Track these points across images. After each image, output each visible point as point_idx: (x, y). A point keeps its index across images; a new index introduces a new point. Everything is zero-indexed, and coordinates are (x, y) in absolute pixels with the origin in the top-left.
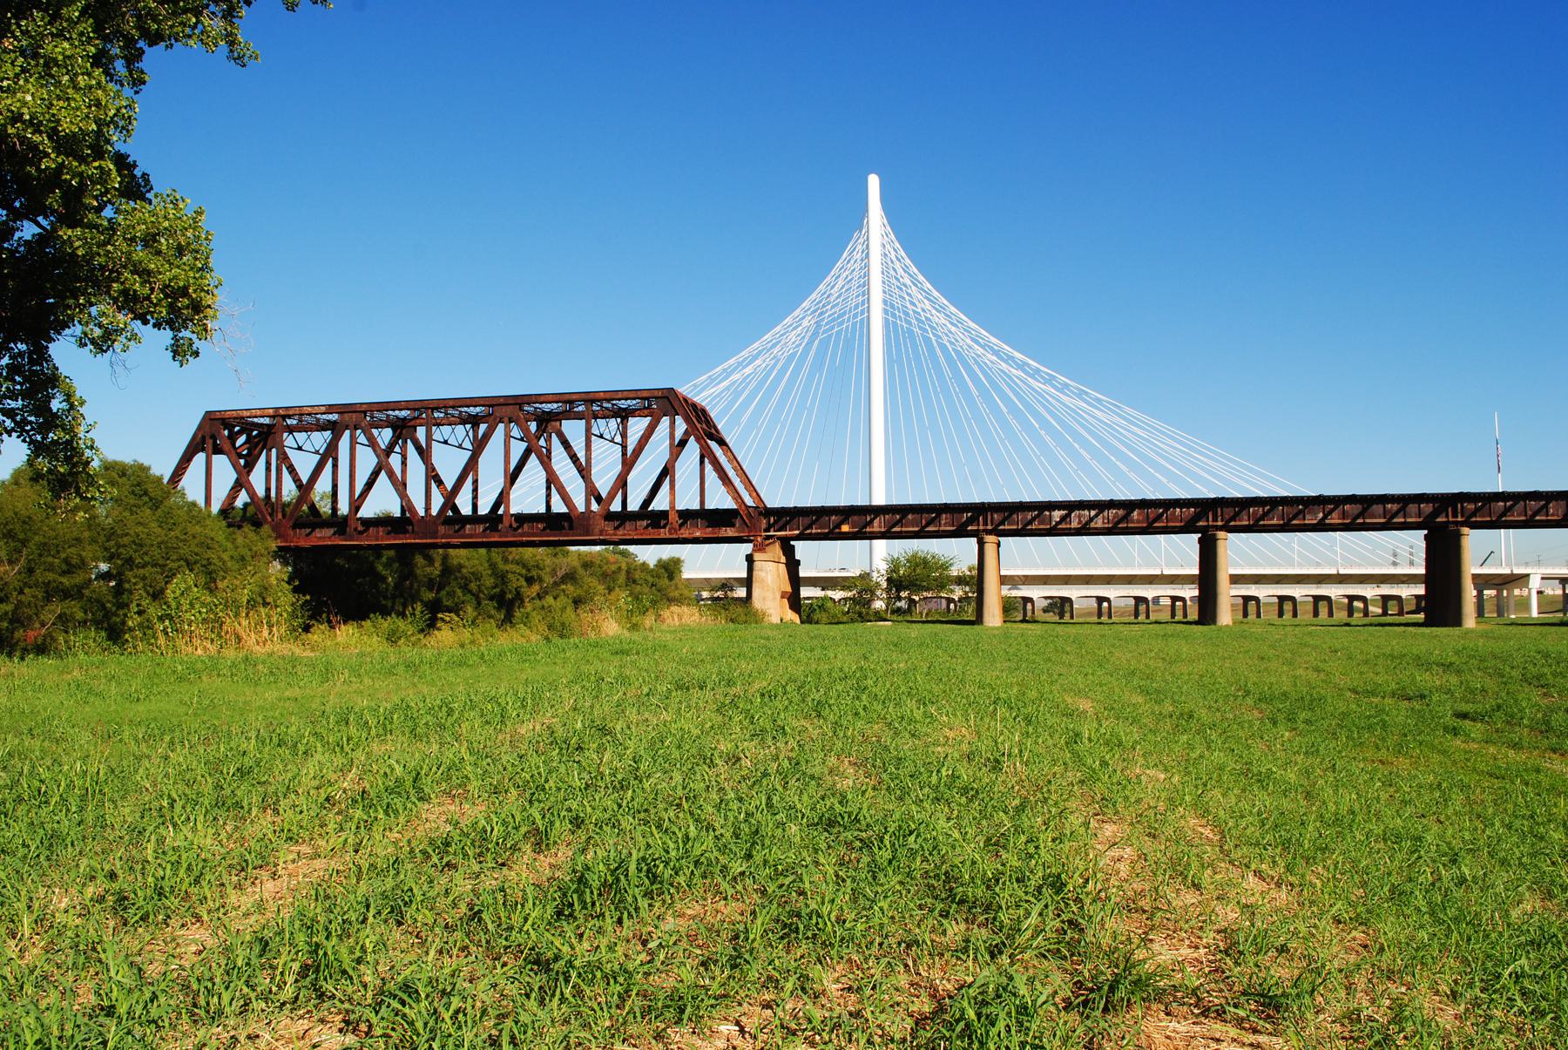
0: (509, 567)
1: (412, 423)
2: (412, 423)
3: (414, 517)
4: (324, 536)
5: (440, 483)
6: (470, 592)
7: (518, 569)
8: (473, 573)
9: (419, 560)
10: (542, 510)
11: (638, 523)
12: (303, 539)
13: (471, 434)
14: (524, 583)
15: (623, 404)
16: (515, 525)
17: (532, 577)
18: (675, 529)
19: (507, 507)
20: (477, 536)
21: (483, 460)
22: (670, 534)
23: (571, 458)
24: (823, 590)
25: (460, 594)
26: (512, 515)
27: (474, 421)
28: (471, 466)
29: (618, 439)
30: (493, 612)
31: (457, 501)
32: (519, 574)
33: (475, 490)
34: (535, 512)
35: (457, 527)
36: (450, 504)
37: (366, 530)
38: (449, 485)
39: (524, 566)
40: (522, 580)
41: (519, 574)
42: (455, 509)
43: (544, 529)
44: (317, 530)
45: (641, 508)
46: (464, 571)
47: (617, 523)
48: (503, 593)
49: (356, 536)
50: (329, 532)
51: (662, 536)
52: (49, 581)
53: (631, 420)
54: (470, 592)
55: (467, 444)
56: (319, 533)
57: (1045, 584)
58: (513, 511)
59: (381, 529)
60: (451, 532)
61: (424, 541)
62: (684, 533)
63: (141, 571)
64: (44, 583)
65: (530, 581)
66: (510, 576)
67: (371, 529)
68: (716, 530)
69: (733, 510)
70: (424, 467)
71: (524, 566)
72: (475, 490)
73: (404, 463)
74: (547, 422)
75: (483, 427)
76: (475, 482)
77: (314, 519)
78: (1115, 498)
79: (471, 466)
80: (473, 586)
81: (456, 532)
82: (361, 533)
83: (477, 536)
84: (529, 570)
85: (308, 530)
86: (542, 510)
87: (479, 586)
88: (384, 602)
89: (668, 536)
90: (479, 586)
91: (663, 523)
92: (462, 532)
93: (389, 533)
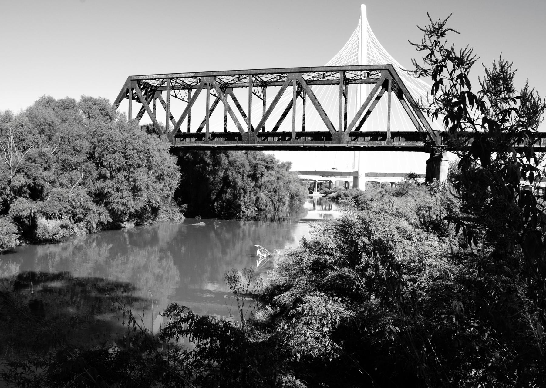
0: (258, 162)
1: (231, 86)
2: (231, 86)
3: (242, 132)
4: (190, 142)
5: (172, 118)
6: (240, 173)
7: (263, 163)
8: (241, 164)
9: (223, 156)
10: (223, 131)
11: (366, 138)
12: (180, 143)
13: (188, 94)
14: (266, 170)
15: (265, 78)
16: (211, 138)
17: (269, 167)
18: (390, 142)
19: (207, 129)
20: (274, 143)
21: (193, 109)
22: (388, 144)
23: (237, 106)
24: (323, 177)
25: (235, 174)
26: (210, 133)
27: (189, 88)
28: (187, 111)
29: (262, 97)
30: (250, 183)
31: (180, 128)
32: (263, 165)
33: (189, 121)
34: (317, 131)
35: (263, 138)
36: (177, 130)
37: (214, 138)
38: (177, 120)
39: (265, 161)
40: (264, 168)
41: (263, 165)
42: (179, 131)
43: (312, 140)
44: (187, 138)
45: (197, 131)
46: (237, 163)
47: (353, 138)
48: (255, 174)
49: (210, 142)
50: (193, 139)
51: (383, 145)
52: (65, 160)
53: (268, 88)
54: (240, 173)
55: (186, 99)
56: (188, 140)
57: (385, 176)
58: (211, 131)
59: (221, 139)
60: (260, 140)
61: (248, 145)
62: (396, 144)
63: (113, 156)
64: (62, 160)
65: (268, 168)
66: (259, 166)
67: (216, 138)
68: (415, 143)
69: (237, 133)
70: (165, 112)
71: (265, 161)
72: (189, 121)
73: (155, 108)
74: (225, 88)
75: (194, 91)
76: (189, 117)
77: (179, 134)
78: (381, 131)
79: (187, 111)
80: (241, 170)
81: (262, 140)
82: (211, 140)
83: (274, 143)
84: (267, 163)
85: (182, 139)
86: (223, 131)
87: (243, 170)
88: (208, 177)
89: (386, 145)
90: (243, 170)
91: (287, 138)
92: (266, 140)
93: (226, 140)
